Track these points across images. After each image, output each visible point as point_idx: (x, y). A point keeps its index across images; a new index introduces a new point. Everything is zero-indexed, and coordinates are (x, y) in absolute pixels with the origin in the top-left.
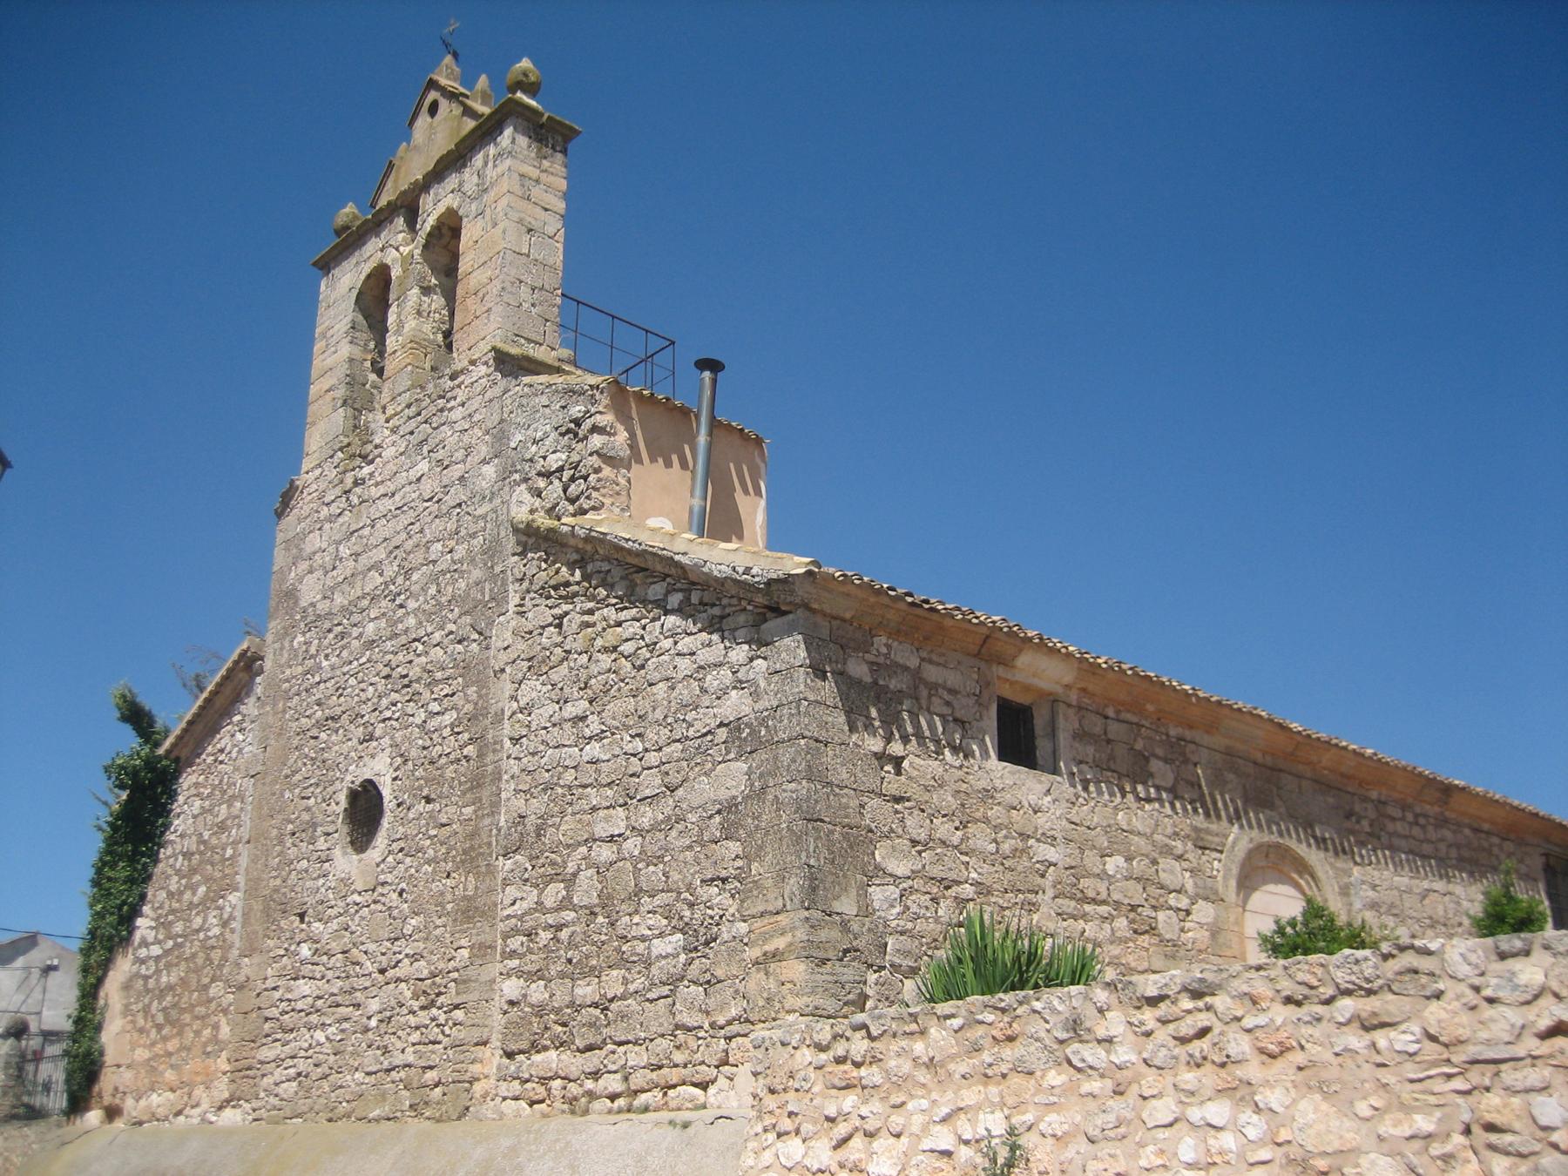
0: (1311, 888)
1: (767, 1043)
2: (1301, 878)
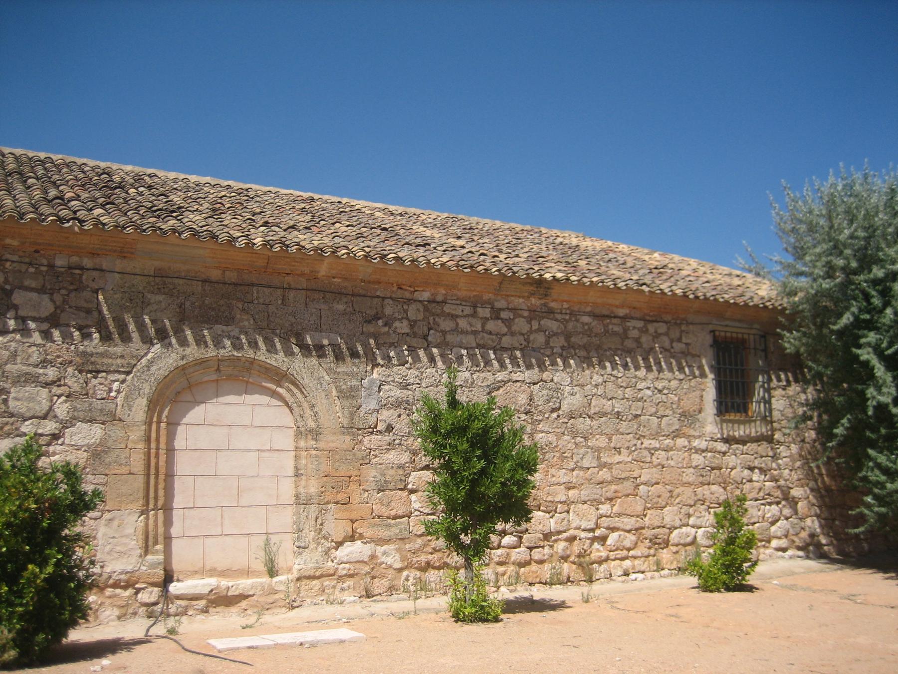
0: (293, 395)
1: (645, 398)
2: (281, 387)
